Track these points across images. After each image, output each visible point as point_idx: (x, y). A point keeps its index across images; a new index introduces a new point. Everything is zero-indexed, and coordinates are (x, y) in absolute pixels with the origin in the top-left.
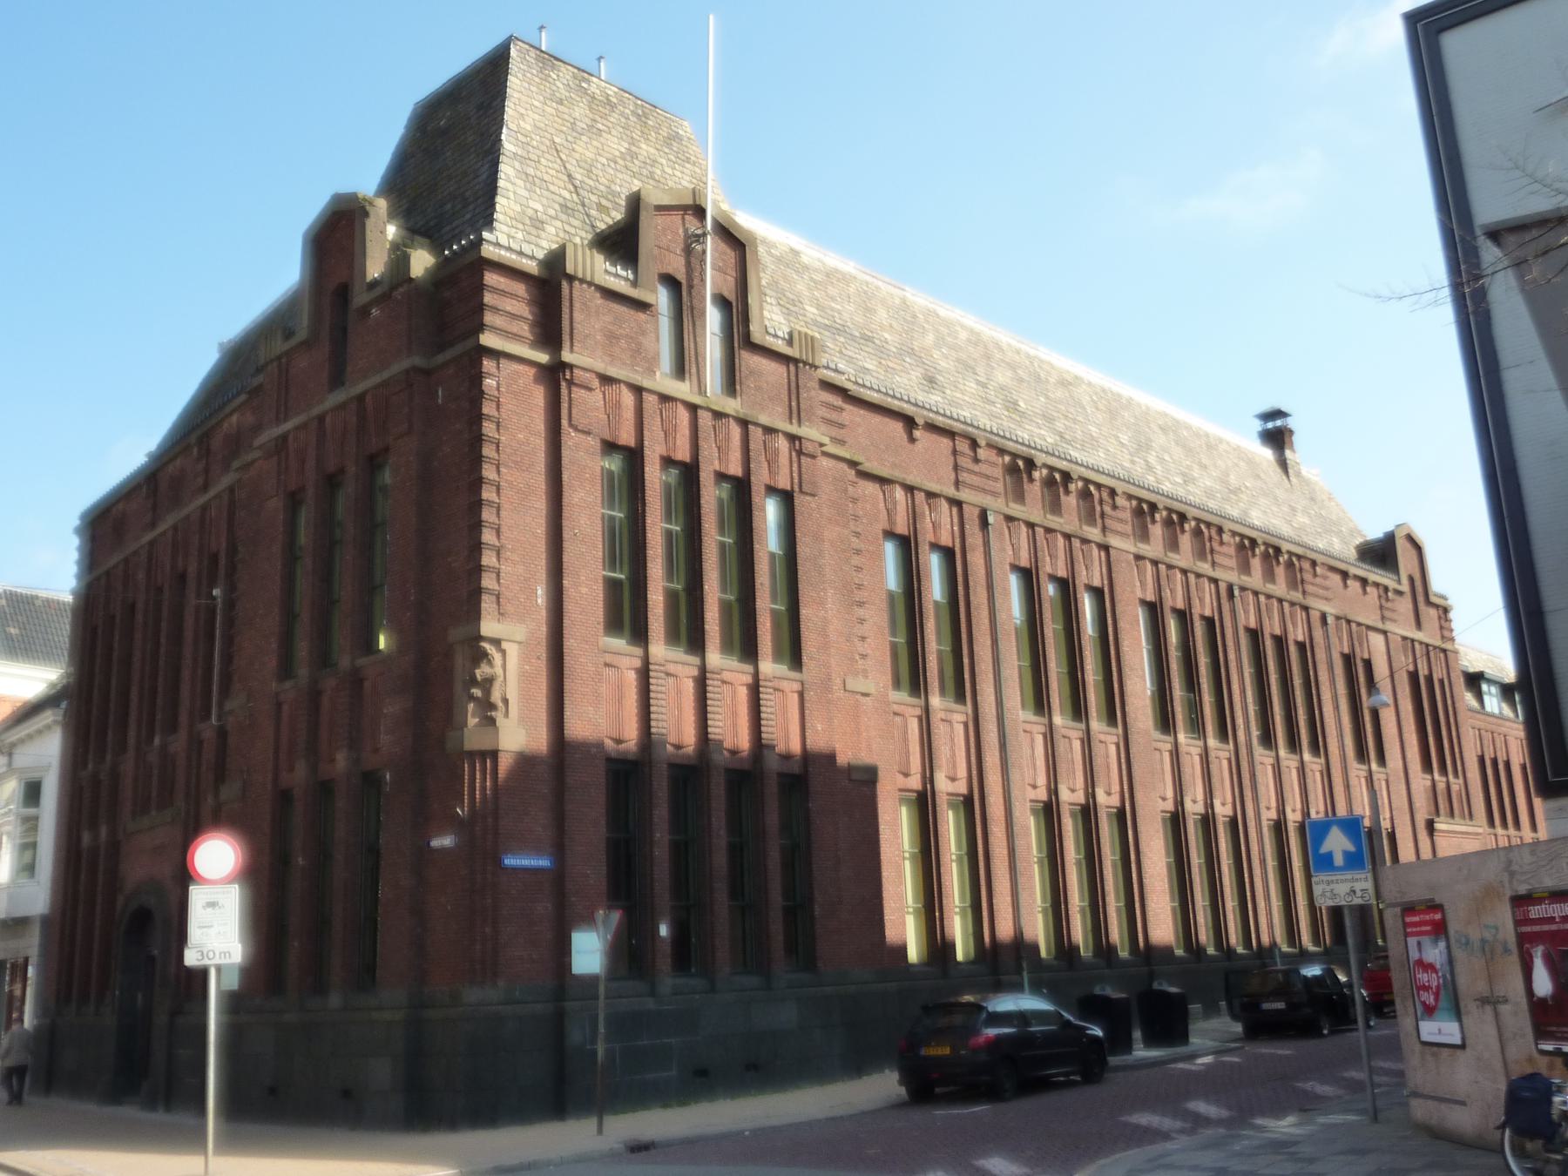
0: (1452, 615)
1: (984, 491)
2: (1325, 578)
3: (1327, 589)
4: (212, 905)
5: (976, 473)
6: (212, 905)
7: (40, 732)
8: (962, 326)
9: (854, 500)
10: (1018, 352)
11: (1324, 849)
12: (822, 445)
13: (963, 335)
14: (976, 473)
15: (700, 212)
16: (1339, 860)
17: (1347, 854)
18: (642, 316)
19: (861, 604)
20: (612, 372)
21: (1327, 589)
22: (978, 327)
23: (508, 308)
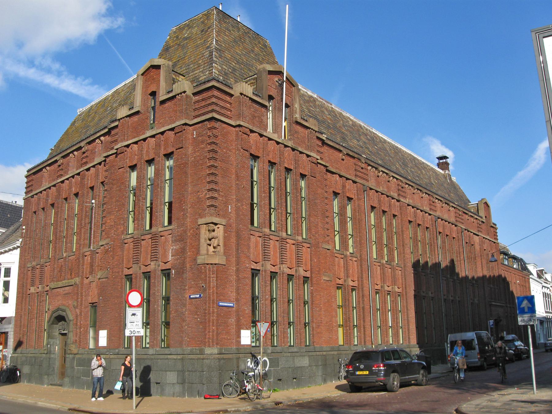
0: (498, 231)
1: (364, 179)
2: (462, 216)
3: (462, 219)
4: (134, 314)
5: (361, 172)
6: (134, 314)
7: (10, 250)
8: (350, 119)
9: (326, 180)
10: (367, 130)
11: (522, 306)
12: (317, 159)
13: (351, 123)
14: (361, 172)
15: (280, 73)
16: (526, 310)
17: (528, 308)
18: (263, 110)
19: (327, 217)
20: (254, 129)
21: (462, 219)
22: (355, 120)
23: (221, 104)
